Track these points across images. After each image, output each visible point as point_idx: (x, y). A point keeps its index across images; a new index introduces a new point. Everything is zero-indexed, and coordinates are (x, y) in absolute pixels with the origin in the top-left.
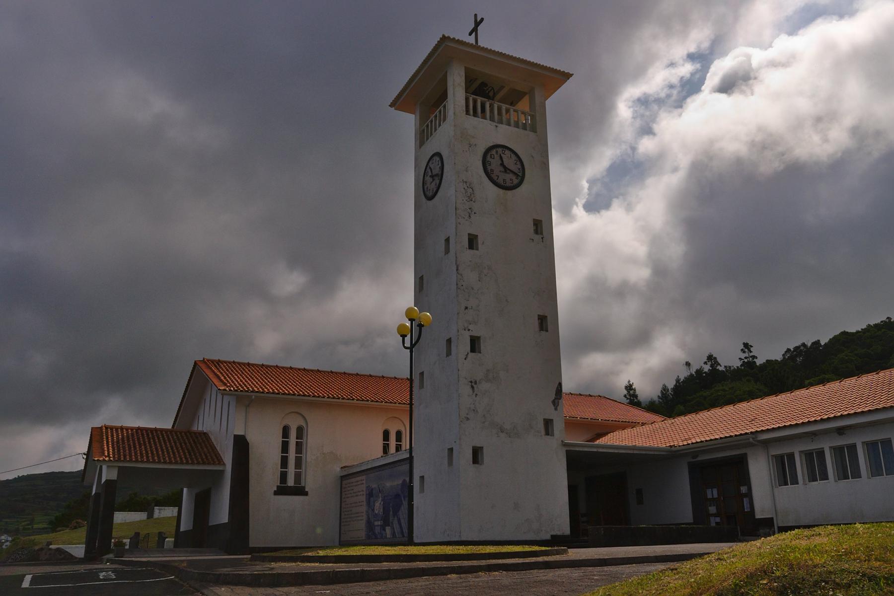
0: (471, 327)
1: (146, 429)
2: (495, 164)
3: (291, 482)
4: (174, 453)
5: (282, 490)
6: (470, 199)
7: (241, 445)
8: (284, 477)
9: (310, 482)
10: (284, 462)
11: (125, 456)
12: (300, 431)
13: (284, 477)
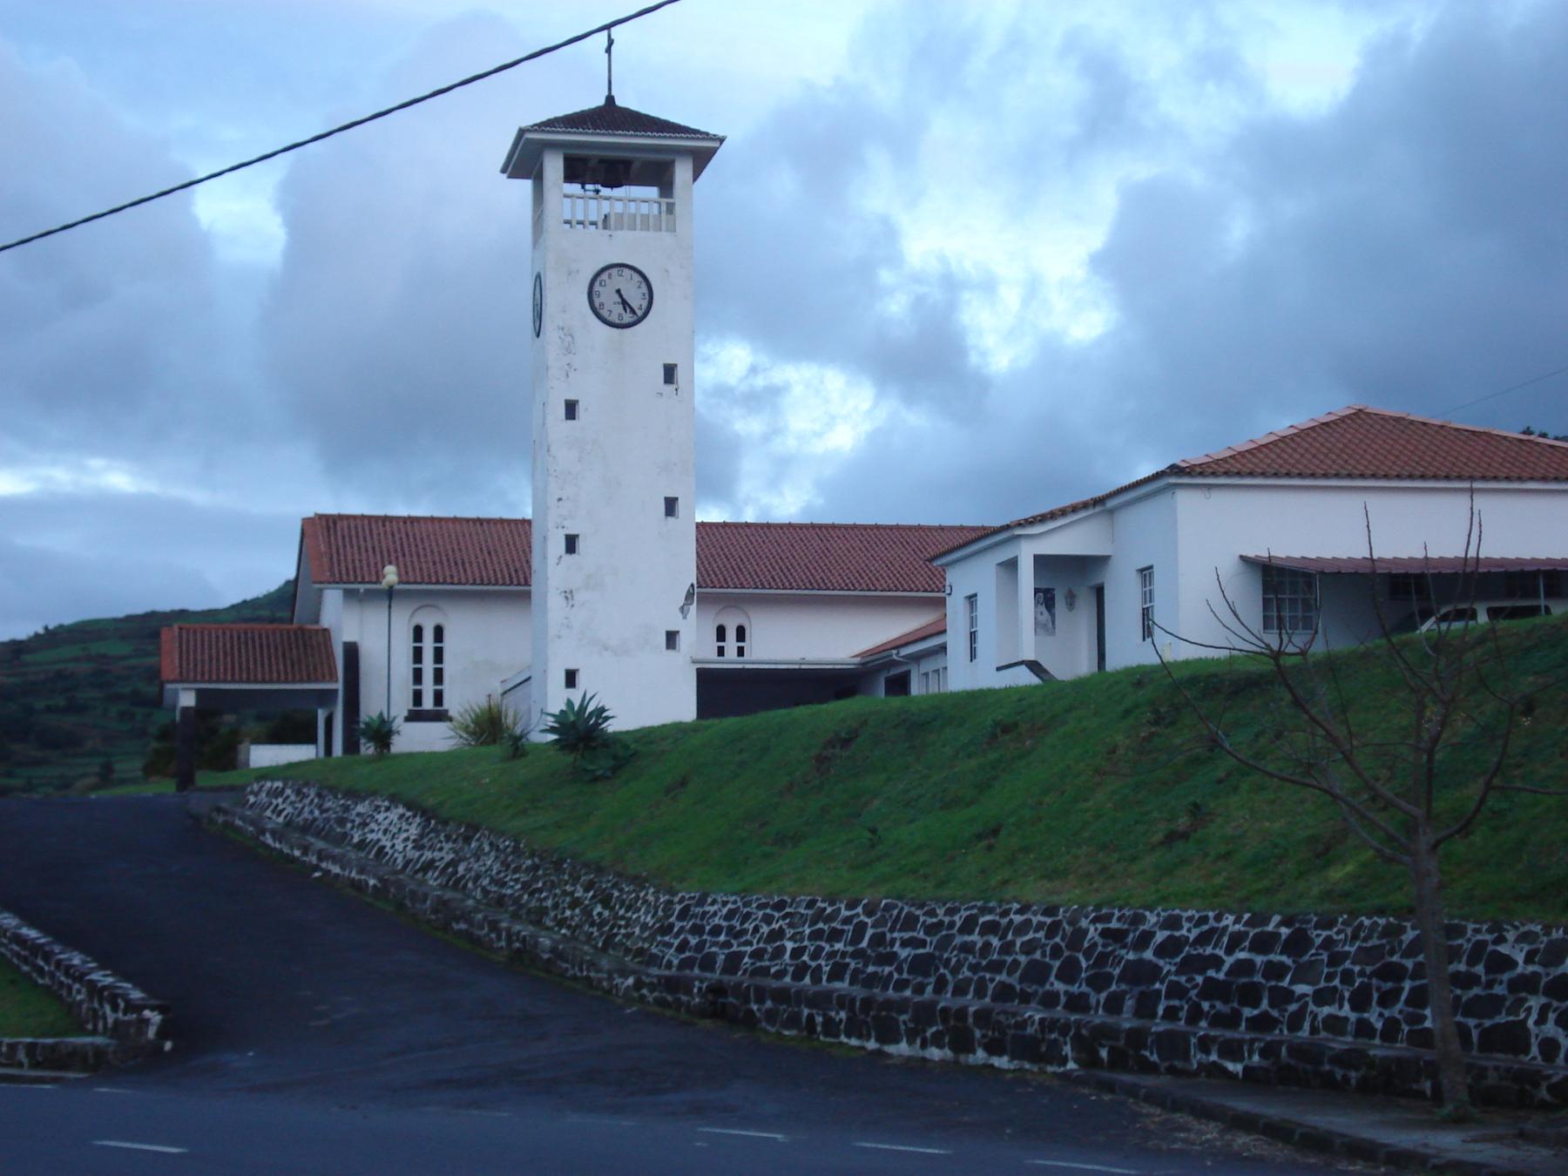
0: (565, 523)
1: (370, 518)
2: (607, 297)
3: (428, 703)
4: (270, 666)
5: (415, 716)
6: (568, 351)
7: (352, 651)
8: (418, 697)
9: (452, 704)
10: (418, 676)
11: (203, 675)
12: (439, 633)
13: (418, 697)
